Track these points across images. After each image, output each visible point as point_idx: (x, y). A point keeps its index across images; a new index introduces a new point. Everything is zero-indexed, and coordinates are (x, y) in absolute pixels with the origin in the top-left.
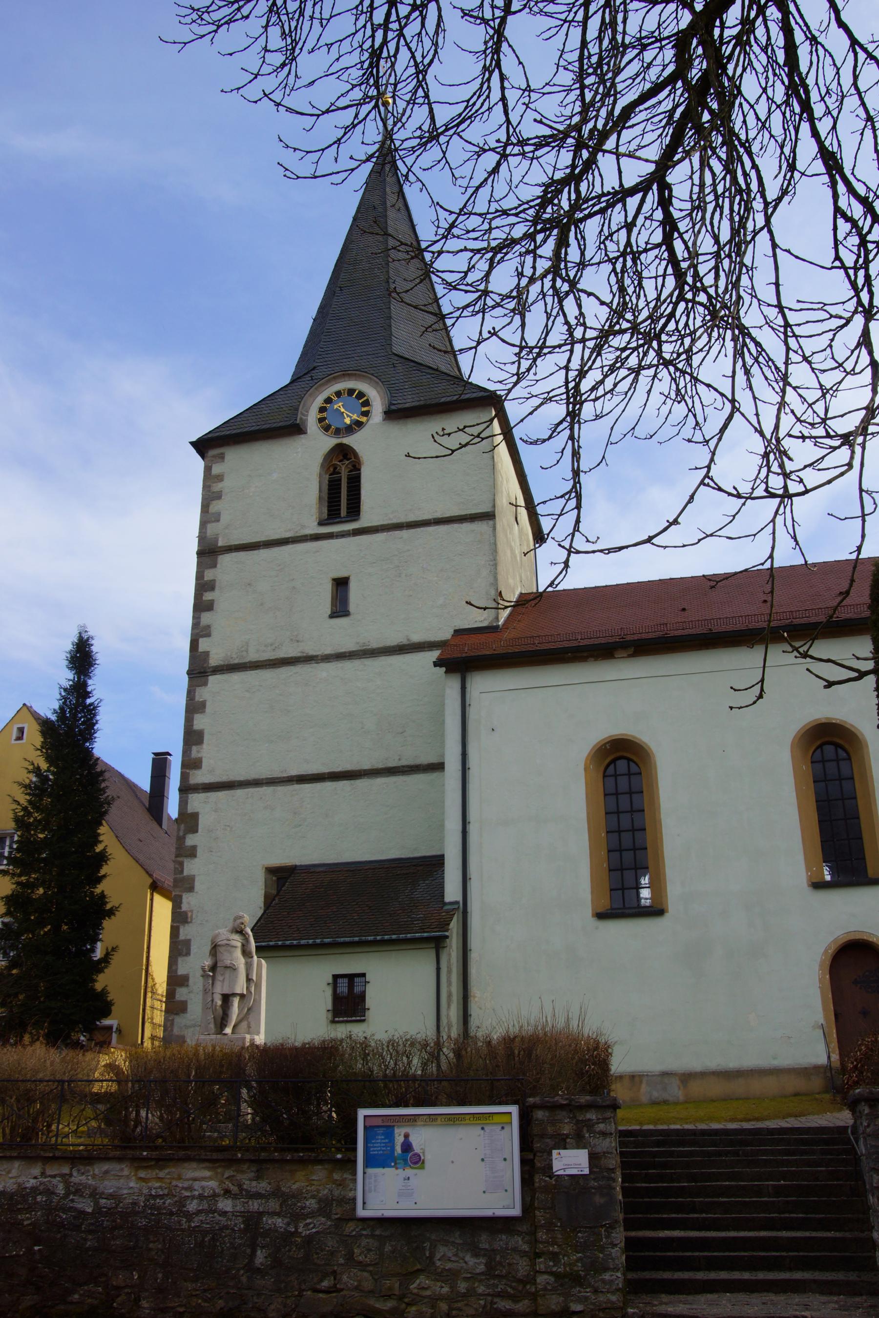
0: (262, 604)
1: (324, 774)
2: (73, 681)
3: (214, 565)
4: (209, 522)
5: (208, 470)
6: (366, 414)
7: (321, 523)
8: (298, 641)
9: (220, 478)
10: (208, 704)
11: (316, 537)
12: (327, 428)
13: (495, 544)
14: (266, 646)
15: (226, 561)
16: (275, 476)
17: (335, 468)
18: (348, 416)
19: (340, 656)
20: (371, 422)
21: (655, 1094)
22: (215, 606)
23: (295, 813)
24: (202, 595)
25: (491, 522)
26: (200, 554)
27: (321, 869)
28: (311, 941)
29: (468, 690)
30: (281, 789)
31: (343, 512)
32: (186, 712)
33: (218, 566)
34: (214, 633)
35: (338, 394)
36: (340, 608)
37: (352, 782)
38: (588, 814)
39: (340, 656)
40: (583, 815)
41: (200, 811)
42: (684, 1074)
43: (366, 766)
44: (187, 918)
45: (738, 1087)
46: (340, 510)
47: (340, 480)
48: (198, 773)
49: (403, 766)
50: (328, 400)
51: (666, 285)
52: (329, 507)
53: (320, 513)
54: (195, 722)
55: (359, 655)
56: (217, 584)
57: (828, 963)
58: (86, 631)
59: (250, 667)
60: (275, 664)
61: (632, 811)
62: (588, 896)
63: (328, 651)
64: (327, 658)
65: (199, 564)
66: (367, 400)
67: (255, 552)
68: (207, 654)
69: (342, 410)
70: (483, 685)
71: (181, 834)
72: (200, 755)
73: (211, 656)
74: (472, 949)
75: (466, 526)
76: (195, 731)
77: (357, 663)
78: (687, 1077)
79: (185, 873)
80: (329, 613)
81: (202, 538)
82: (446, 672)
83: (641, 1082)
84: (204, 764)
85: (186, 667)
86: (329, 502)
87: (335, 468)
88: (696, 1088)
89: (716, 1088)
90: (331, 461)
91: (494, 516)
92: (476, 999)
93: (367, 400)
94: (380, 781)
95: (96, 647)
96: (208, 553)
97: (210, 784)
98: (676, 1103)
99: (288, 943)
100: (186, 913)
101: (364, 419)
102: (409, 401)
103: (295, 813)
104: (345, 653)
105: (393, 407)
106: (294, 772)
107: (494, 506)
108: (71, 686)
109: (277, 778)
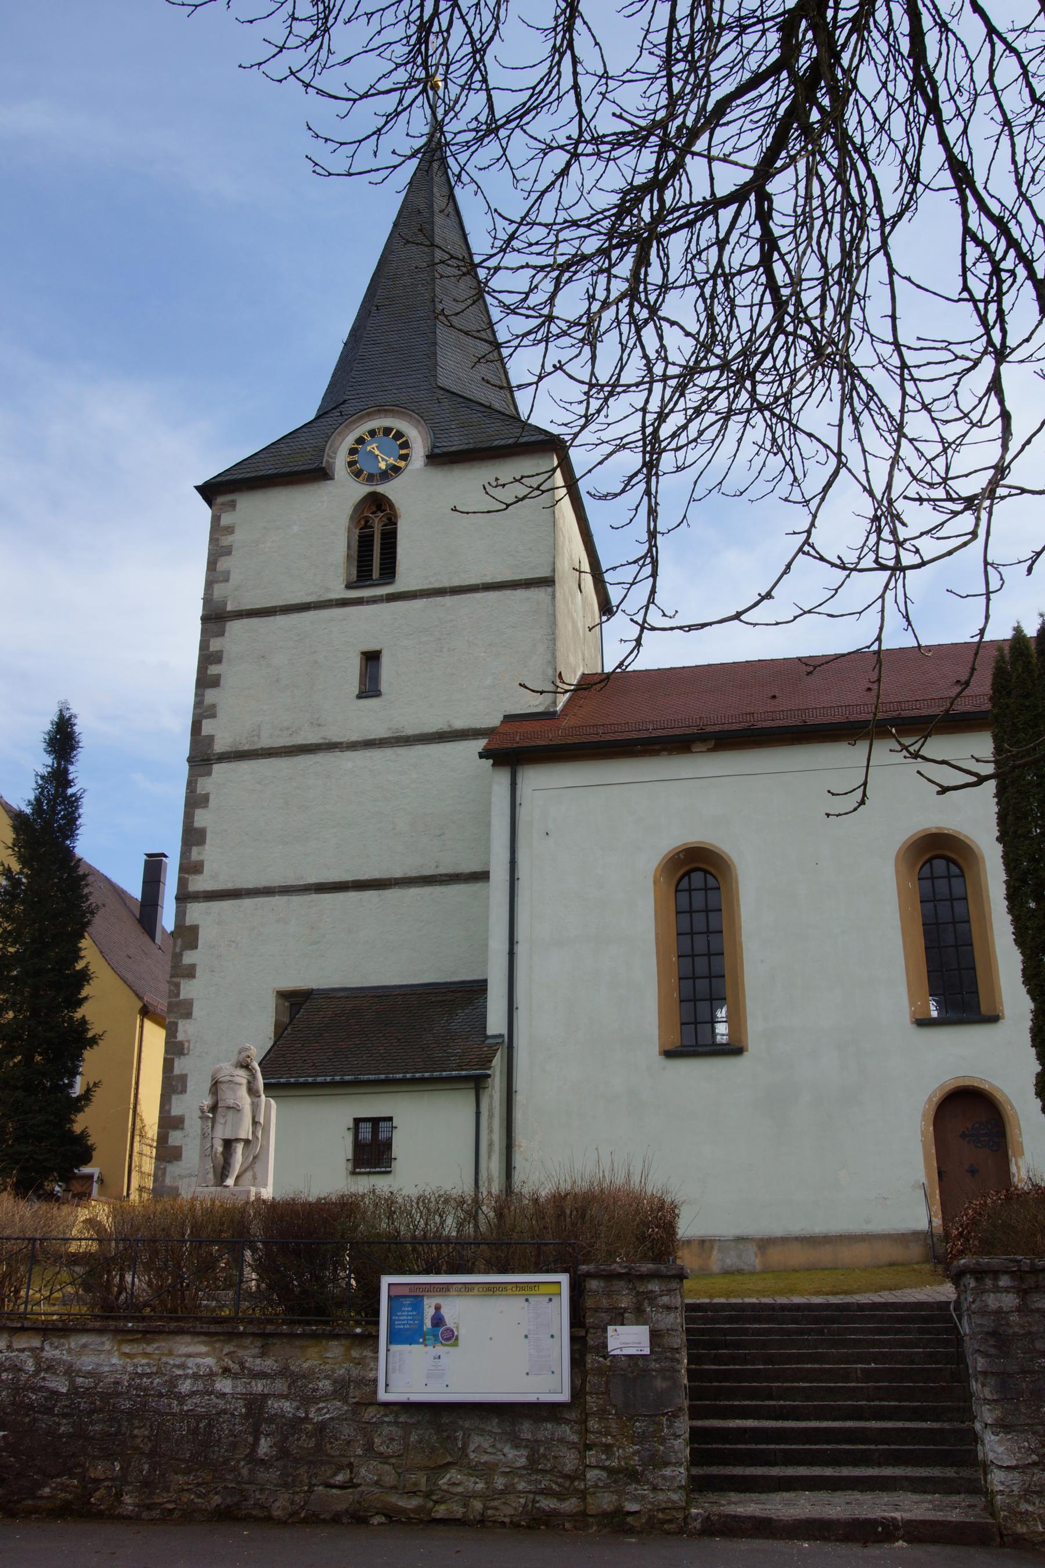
0: (277, 681)
1: (347, 882)
2: (52, 767)
4: (217, 582)
5: (215, 520)
6: (404, 458)
7: (349, 586)
8: (319, 725)
9: (230, 530)
10: (212, 797)
11: (344, 603)
12: (358, 474)
14: (281, 730)
15: (235, 628)
16: (295, 529)
17: (367, 522)
18: (383, 459)
20: (410, 467)
21: (728, 1262)
22: (222, 681)
24: (206, 668)
25: (550, 589)
26: (205, 619)
27: (342, 994)
28: (329, 1079)
29: (519, 786)
30: (296, 900)
31: (376, 574)
33: (226, 634)
35: (372, 433)
36: (369, 687)
37: (380, 892)
40: (652, 936)
42: (762, 1240)
44: (183, 1049)
45: (824, 1255)
46: (371, 570)
47: (372, 535)
49: (441, 875)
50: (360, 441)
52: (358, 567)
53: (348, 574)
54: (196, 819)
57: (932, 1113)
58: (68, 709)
61: (708, 932)
62: (656, 1032)
63: (355, 737)
64: (354, 746)
68: (211, 738)
69: (377, 452)
70: (540, 783)
71: (178, 950)
72: (201, 858)
74: (518, 1089)
75: (520, 594)
76: (196, 829)
77: (389, 753)
78: (765, 1244)
81: (207, 600)
82: (493, 765)
83: (712, 1248)
86: (359, 562)
87: (367, 522)
88: (777, 1256)
89: (799, 1256)
90: (363, 512)
94: (414, 892)
95: (81, 727)
96: (215, 618)
97: (213, 892)
98: (752, 1273)
99: (302, 1080)
100: (181, 1043)
101: (402, 464)
102: (456, 443)
103: (313, 928)
104: (375, 740)
105: (437, 451)
106: (312, 879)
107: (554, 570)
108: (49, 773)
109: (292, 886)
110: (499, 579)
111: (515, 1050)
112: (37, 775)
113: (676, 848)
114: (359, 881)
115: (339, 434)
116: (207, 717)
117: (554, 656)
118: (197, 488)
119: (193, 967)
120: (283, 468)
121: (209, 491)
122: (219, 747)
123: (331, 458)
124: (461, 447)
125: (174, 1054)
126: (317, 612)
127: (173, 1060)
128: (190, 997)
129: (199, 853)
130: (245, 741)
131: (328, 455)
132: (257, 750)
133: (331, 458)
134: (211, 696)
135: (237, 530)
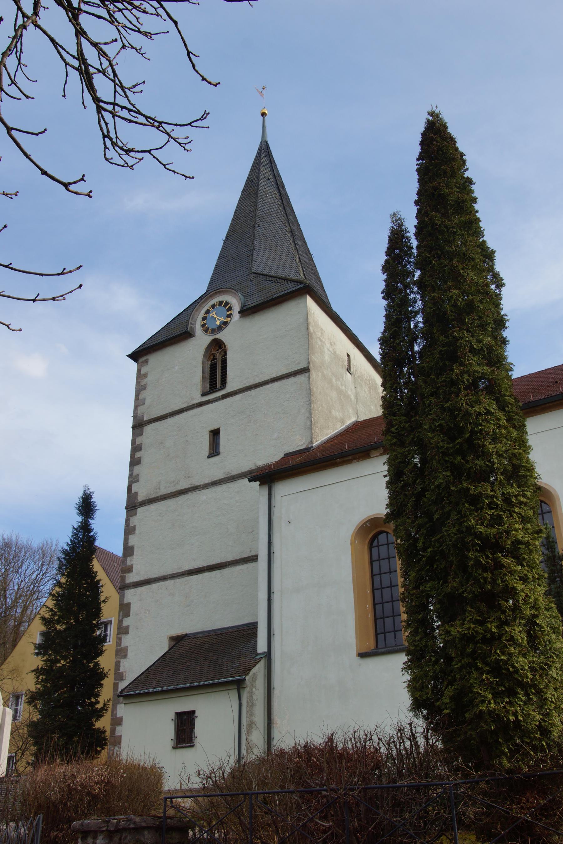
0: (168, 456)
1: (204, 567)
2: (81, 523)
3: (141, 434)
4: (139, 406)
5: (139, 371)
6: (229, 316)
7: (203, 395)
8: (189, 477)
9: (145, 376)
10: (137, 527)
11: (200, 405)
12: (206, 331)
13: (310, 389)
14: (170, 483)
15: (148, 429)
16: (177, 368)
17: (214, 356)
18: (218, 319)
19: (214, 484)
20: (233, 321)
22: (142, 461)
23: (187, 597)
24: (134, 455)
25: (307, 374)
26: (134, 427)
27: (201, 635)
28: (160, 689)
30: (179, 581)
31: (219, 385)
32: (125, 534)
33: (144, 434)
34: (141, 479)
35: (213, 306)
36: (214, 450)
37: (221, 570)
38: (353, 577)
39: (214, 484)
40: (350, 579)
41: (131, 601)
43: (230, 558)
44: (123, 677)
46: (216, 383)
47: (217, 363)
48: (130, 575)
49: (252, 556)
50: (208, 312)
51: (107, 121)
52: (210, 382)
53: (203, 386)
54: (129, 541)
55: (225, 481)
56: (143, 446)
58: (89, 489)
59: (161, 499)
60: (175, 495)
63: (207, 481)
64: (206, 486)
65: (134, 435)
66: (230, 306)
67: (165, 421)
68: (136, 493)
69: (215, 316)
70: (285, 490)
71: (121, 618)
72: (132, 563)
73: (139, 494)
74: (275, 687)
75: (292, 380)
76: (129, 547)
77: (224, 487)
79: (122, 646)
80: (208, 455)
81: (135, 417)
82: (259, 485)
84: (134, 569)
85: (125, 504)
86: (210, 379)
87: (214, 356)
90: (211, 351)
91: (309, 369)
92: (278, 726)
93: (230, 306)
94: (239, 568)
95: (95, 499)
96: (139, 426)
97: (137, 582)
99: (146, 691)
100: (122, 673)
101: (228, 320)
102: (254, 301)
103: (187, 597)
104: (217, 481)
105: (245, 308)
106: (186, 568)
107: (309, 363)
108: (79, 526)
109: (176, 573)
110: (280, 374)
111: (273, 661)
112: (74, 528)
113: (363, 520)
114: (210, 565)
115: (196, 311)
116: (134, 482)
117: (310, 414)
118: (129, 356)
119: (128, 627)
120: (174, 335)
121: (135, 356)
122: (140, 498)
123: (193, 324)
124: (257, 303)
125: (118, 680)
126: (187, 412)
127: (118, 683)
128: (126, 645)
129: (131, 561)
130: (152, 493)
131: (191, 323)
132: (158, 497)
133: (193, 324)
134: (137, 469)
135: (149, 376)
